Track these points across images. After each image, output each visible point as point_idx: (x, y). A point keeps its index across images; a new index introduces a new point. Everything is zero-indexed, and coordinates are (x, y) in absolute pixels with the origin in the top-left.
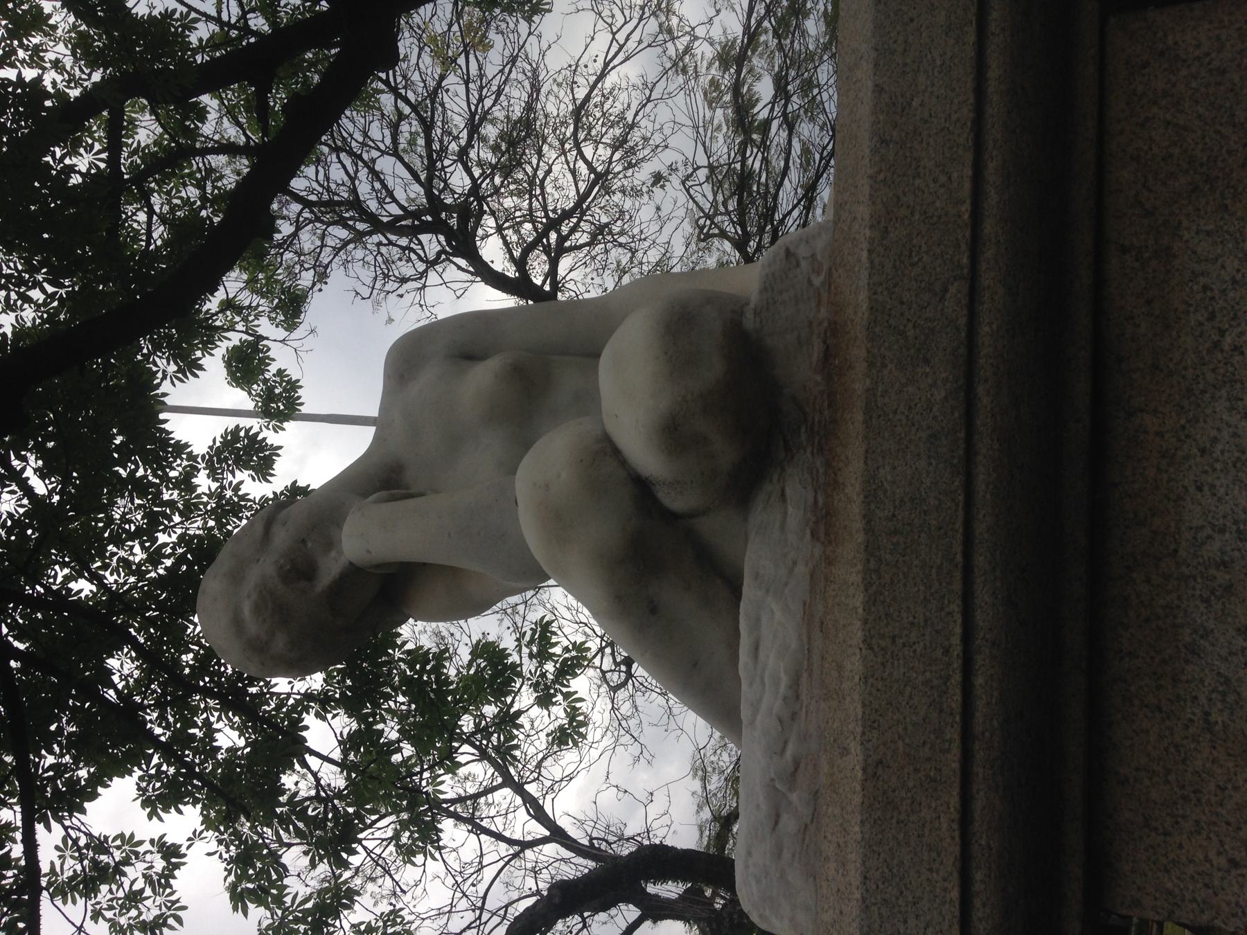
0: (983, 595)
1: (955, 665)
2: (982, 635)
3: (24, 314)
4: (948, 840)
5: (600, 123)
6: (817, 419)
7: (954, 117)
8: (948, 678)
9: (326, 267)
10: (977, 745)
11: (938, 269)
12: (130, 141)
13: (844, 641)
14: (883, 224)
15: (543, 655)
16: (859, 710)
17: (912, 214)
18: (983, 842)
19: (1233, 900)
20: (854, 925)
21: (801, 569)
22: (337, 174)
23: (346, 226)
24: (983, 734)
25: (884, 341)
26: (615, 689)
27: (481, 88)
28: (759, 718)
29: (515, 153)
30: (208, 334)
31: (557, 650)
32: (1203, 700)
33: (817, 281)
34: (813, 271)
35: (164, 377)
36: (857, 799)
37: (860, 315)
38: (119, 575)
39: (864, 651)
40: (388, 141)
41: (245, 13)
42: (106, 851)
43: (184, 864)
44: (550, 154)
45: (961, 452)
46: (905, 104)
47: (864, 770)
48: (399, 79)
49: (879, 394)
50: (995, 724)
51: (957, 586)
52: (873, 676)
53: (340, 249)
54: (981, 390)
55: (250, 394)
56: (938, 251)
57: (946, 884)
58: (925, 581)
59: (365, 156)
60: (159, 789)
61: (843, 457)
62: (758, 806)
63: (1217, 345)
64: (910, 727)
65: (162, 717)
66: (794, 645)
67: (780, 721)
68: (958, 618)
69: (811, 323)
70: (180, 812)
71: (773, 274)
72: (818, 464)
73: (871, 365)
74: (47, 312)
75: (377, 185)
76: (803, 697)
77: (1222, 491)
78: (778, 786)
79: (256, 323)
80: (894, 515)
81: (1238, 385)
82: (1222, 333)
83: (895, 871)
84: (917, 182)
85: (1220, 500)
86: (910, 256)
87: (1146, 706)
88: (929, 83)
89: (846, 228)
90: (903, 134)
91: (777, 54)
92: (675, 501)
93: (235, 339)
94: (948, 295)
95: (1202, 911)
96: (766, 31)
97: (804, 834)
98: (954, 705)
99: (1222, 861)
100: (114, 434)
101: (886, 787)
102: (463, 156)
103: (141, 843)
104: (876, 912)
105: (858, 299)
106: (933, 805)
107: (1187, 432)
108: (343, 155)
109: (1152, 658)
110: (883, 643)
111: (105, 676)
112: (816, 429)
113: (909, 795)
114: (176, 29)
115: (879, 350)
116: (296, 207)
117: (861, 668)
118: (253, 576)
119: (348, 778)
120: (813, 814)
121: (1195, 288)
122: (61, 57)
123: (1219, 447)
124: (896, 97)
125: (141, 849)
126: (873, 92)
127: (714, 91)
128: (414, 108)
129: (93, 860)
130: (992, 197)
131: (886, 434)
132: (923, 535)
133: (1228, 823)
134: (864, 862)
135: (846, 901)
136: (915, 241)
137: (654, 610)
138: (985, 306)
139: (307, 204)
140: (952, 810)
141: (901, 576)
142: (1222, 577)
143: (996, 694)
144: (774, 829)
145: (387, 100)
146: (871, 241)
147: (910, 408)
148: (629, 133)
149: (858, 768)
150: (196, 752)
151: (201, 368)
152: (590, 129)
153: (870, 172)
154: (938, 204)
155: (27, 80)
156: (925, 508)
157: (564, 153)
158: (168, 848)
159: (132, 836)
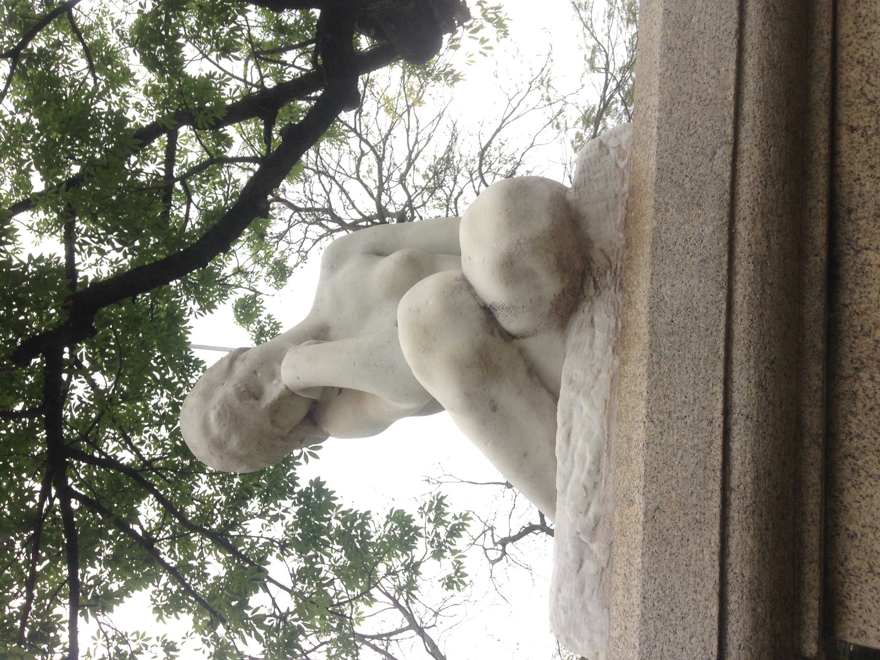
0: (740, 379)
1: (717, 433)
3: (102, 268)
4: (709, 569)
5: (498, 161)
6: (619, 266)
7: (722, 28)
8: (711, 443)
9: (307, 252)
12: (181, 159)
13: (633, 419)
15: (438, 521)
18: (737, 571)
20: (635, 636)
21: (604, 376)
22: (317, 189)
23: (322, 225)
24: (738, 487)
25: (668, 192)
26: (493, 562)
27: (418, 134)
28: (569, 487)
29: (438, 179)
30: (225, 288)
31: (447, 518)
33: (622, 164)
34: (619, 157)
35: (191, 313)
36: (640, 537)
37: (650, 175)
38: (150, 449)
40: (354, 170)
41: (262, 77)
42: (126, 642)
43: (178, 656)
44: (462, 180)
45: (725, 272)
46: (686, 21)
47: (645, 514)
48: (363, 128)
50: (748, 479)
51: (720, 373)
53: (317, 241)
54: (740, 226)
55: (248, 330)
56: (709, 124)
57: (708, 603)
58: (695, 369)
59: (337, 178)
60: (165, 601)
61: (636, 283)
62: (567, 554)
64: (681, 480)
65: (172, 551)
66: (597, 431)
68: (720, 396)
69: (616, 196)
70: (178, 618)
71: (590, 160)
73: (657, 210)
74: (117, 267)
75: (344, 197)
76: (603, 471)
78: (582, 538)
79: (256, 283)
83: (667, 592)
87: (871, 476)
88: (704, 5)
89: (642, 116)
90: (685, 42)
91: (624, 116)
92: (511, 323)
93: (241, 293)
94: (716, 156)
96: (617, 101)
97: (601, 575)
98: (716, 464)
100: (88, 184)
102: (402, 180)
103: (148, 639)
105: (650, 164)
106: (698, 541)
108: (323, 177)
110: (661, 417)
111: (134, 516)
112: (618, 273)
113: (680, 533)
114: (216, 85)
116: (289, 212)
117: (644, 436)
118: (219, 395)
119: (296, 602)
120: (608, 561)
122: (140, 101)
124: (680, 17)
125: (149, 643)
127: (579, 141)
128: (372, 148)
129: (117, 648)
130: (751, 86)
131: (668, 261)
132: (694, 335)
135: (629, 618)
136: (692, 119)
137: (494, 409)
138: (744, 164)
139: (297, 210)
140: (713, 545)
143: (749, 456)
144: (578, 571)
145: (354, 141)
146: (660, 120)
148: (516, 168)
149: (640, 513)
150: (192, 576)
151: (215, 307)
152: (491, 164)
153: (660, 71)
154: (709, 91)
155: (115, 111)
156: (696, 315)
157: (472, 180)
158: (168, 644)
159: (144, 634)
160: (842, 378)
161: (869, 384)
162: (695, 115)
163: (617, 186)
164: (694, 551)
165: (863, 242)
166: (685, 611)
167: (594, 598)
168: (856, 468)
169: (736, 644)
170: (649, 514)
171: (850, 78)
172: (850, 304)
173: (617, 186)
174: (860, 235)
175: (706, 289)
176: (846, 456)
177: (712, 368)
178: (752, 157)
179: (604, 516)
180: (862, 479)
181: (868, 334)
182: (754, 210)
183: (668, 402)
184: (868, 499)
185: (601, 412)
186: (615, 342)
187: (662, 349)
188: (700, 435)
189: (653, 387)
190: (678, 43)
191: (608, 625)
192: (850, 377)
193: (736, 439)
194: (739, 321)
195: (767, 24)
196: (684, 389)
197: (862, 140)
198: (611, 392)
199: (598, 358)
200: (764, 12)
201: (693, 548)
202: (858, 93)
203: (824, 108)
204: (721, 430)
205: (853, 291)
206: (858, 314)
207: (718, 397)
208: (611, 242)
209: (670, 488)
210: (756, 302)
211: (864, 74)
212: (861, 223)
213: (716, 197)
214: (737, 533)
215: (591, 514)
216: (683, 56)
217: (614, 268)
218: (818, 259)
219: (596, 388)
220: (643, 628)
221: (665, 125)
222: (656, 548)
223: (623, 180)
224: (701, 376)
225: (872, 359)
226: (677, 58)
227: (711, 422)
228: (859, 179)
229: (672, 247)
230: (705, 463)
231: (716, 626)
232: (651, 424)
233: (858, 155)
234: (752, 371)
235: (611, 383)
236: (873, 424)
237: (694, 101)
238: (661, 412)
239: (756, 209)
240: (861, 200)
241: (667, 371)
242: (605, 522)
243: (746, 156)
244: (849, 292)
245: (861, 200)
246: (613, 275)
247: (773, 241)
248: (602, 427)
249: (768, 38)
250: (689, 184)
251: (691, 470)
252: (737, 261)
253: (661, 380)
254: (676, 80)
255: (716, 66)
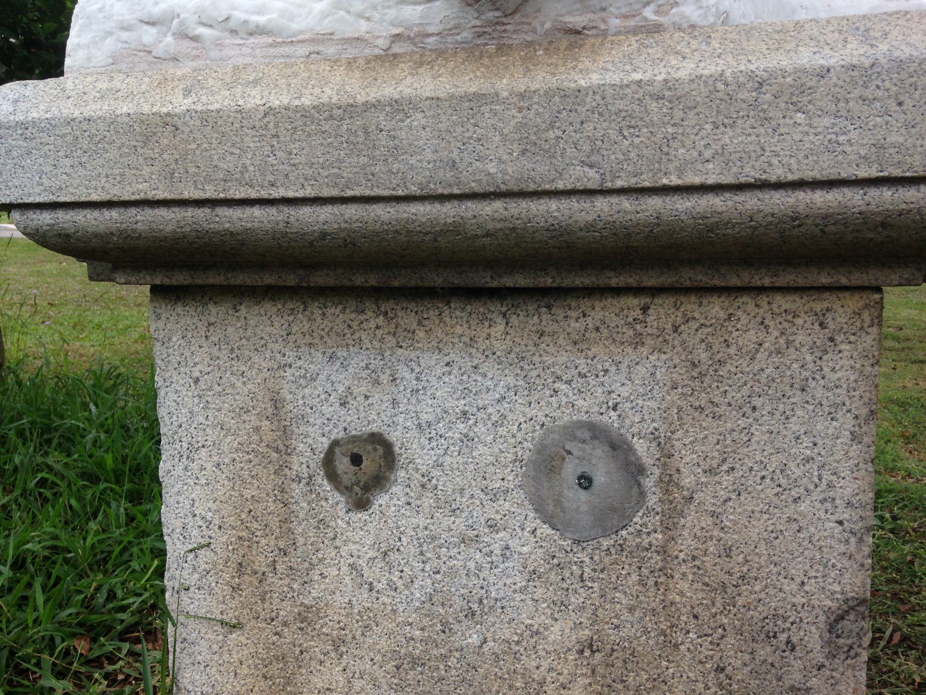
1: (262, 192)
2: (292, 213)
6: (508, 27)
7: (775, 161)
10: (207, 210)
11: (613, 157)
14: (667, 93)
16: (216, 106)
17: (674, 125)
19: (174, 380)
21: (363, 26)
25: (545, 108)
32: (300, 363)
34: (660, 6)
36: (146, 109)
39: (262, 108)
45: (440, 191)
47: (168, 114)
49: (493, 107)
50: (227, 225)
51: (326, 193)
52: (243, 118)
54: (498, 204)
56: (632, 155)
63: (559, 378)
64: (208, 154)
66: (294, 26)
67: (227, 19)
68: (300, 194)
69: (603, 9)
72: (464, 34)
73: (522, 96)
76: (252, 40)
77: (447, 380)
80: (381, 131)
81: (526, 393)
82: (569, 382)
84: (708, 127)
85: (440, 378)
86: (630, 127)
88: (820, 130)
90: (765, 107)
94: (587, 169)
95: (163, 360)
98: (231, 192)
99: (197, 374)
101: (159, 134)
104: (67, 131)
107: (491, 356)
109: (323, 329)
110: (271, 126)
112: (498, 28)
113: (157, 156)
115: (538, 103)
120: (159, 58)
121: (607, 364)
123: (479, 379)
124: (809, 94)
126: (822, 67)
131: (455, 118)
133: (221, 378)
134: (100, 118)
136: (645, 130)
138: (576, 204)
140: (153, 192)
141: (330, 140)
142: (385, 378)
143: (249, 225)
144: (141, 21)
147: (480, 140)
153: (728, 73)
154: (682, 151)
156: (390, 160)
160: (377, 300)
161: (372, 324)
162: (649, 134)
163: (618, 8)
164: (144, 172)
165: (514, 320)
166: (88, 165)
167: (120, 45)
168: (295, 312)
169: (77, 218)
170: (169, 119)
171: (712, 305)
172: (450, 308)
173: (618, 8)
174: (522, 317)
175: (421, 170)
176: (304, 303)
177: (331, 184)
178: (583, 214)
179: (204, 48)
180: (286, 317)
181: (420, 323)
182: (517, 219)
183: (289, 133)
184: (269, 323)
185: (318, 29)
186: (409, 36)
187: (348, 121)
188: (257, 174)
189: (304, 113)
190: (768, 95)
191: (99, 65)
192: (379, 308)
193: (262, 211)
194: (388, 210)
195: (772, 219)
196: (304, 152)
197: (630, 319)
198: (344, 39)
199: (385, 14)
200: (792, 214)
201: (146, 170)
202: (690, 315)
203: (669, 280)
204: (266, 196)
205: (463, 310)
206: (440, 315)
207: (300, 191)
208: (539, 11)
209: (199, 142)
210: (411, 227)
211: (714, 321)
212: (535, 318)
213: (532, 173)
214: (173, 215)
215: (201, 30)
216: (744, 105)
217: (505, 20)
218: (488, 279)
219: (348, 17)
220: (62, 120)
221: (641, 91)
222: (138, 129)
223: (625, 17)
224: (320, 170)
225: (396, 327)
226: (743, 97)
227: (272, 185)
228: (584, 316)
229: (472, 121)
230: (231, 181)
231: (83, 199)
232: (263, 113)
233: (612, 315)
234: (336, 226)
235: (355, 38)
236: (336, 327)
237: (670, 130)
238: (277, 125)
239: (519, 222)
240: (560, 318)
241: (323, 129)
242: (197, 49)
243: (585, 205)
244: (462, 306)
245: (559, 318)
246: (496, 20)
247: (485, 240)
248: (301, 32)
249: (752, 221)
250: (553, 136)
251: (221, 164)
252: (456, 203)
253: (312, 122)
254: (708, 100)
255: (716, 156)
